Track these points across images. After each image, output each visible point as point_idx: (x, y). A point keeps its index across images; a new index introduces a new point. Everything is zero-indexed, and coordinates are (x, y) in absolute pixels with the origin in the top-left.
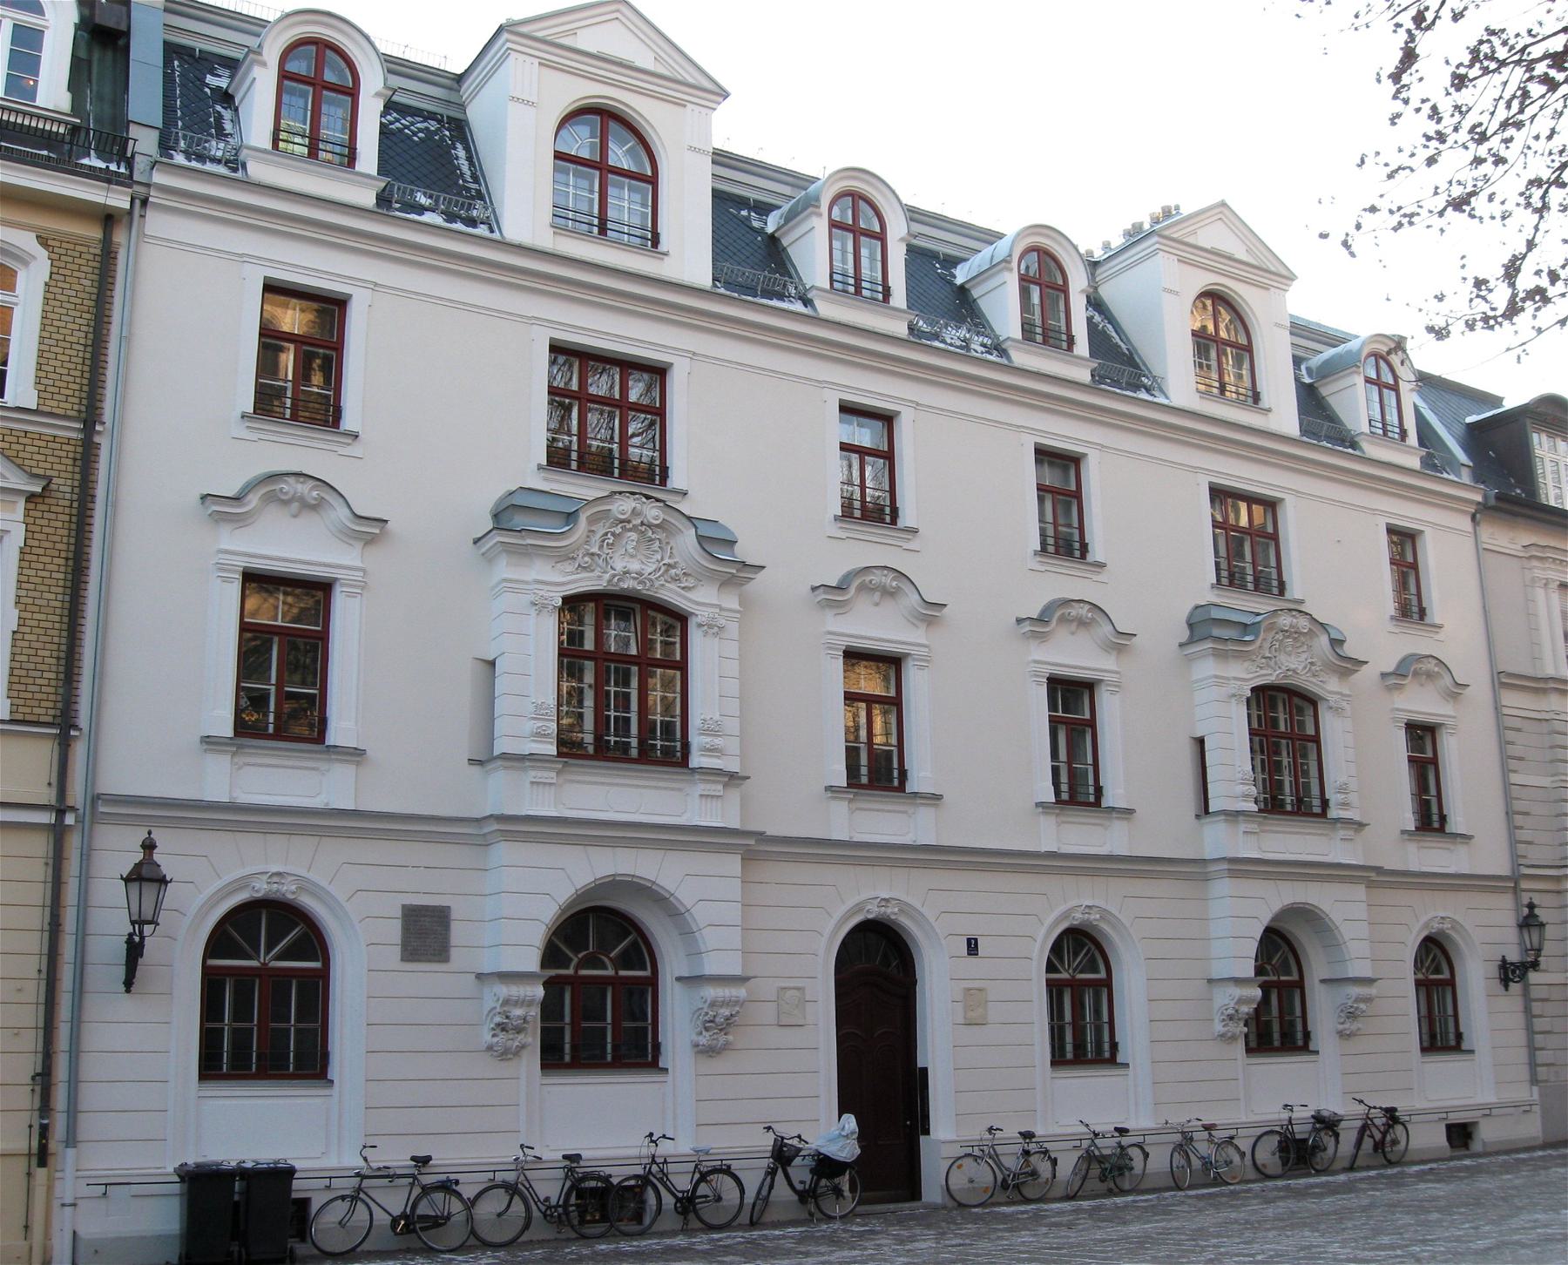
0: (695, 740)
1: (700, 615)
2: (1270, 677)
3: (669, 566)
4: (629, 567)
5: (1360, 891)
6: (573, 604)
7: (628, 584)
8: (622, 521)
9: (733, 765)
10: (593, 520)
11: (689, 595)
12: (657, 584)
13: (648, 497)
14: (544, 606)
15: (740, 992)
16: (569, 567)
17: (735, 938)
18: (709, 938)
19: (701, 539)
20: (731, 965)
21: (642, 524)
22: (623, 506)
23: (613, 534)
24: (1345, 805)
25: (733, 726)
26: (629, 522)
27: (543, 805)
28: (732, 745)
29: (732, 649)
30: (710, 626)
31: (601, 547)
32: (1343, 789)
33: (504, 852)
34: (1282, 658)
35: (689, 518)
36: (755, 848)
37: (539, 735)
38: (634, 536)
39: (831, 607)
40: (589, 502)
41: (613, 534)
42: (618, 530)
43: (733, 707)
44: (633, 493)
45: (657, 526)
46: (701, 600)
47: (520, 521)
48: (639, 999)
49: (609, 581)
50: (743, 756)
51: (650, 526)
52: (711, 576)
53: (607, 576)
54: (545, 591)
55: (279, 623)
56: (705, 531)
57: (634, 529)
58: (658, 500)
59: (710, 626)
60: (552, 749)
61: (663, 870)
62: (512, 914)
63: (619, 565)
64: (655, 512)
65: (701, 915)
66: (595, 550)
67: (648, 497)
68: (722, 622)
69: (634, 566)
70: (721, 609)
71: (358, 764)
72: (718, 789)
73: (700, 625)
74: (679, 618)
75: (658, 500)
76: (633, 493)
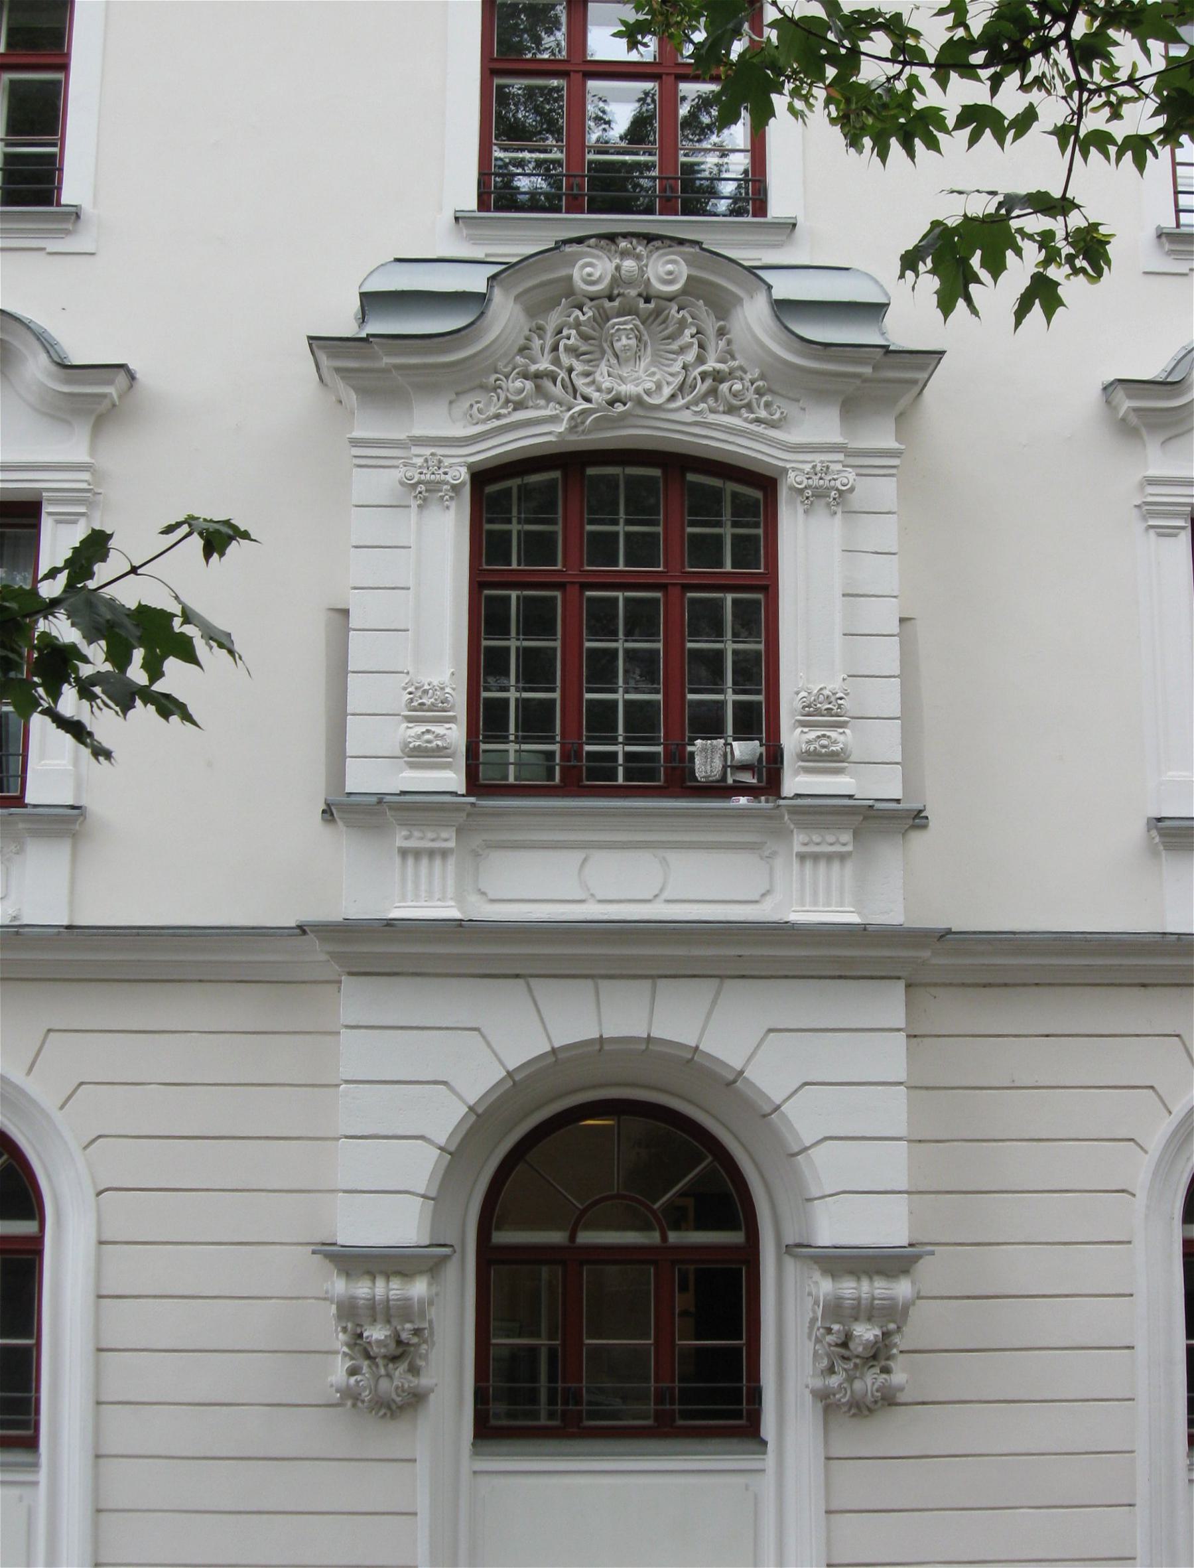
0: (792, 738)
1: (796, 474)
2: (544, 428)
3: (718, 377)
4: (643, 389)
5: (888, 1006)
9: (885, 786)
14: (433, 487)
15: (902, 1289)
17: (893, 1165)
18: (826, 1168)
20: (887, 1227)
22: (594, 269)
24: (826, 759)
25: (886, 697)
27: (426, 895)
28: (885, 741)
32: (825, 713)
33: (356, 1002)
34: (727, 370)
36: (949, 970)
37: (420, 755)
39: (1153, 428)
40: (511, 266)
43: (887, 656)
44: (612, 238)
46: (799, 440)
48: (724, 1299)
49: (572, 429)
50: (910, 763)
56: (786, 287)
60: (453, 779)
61: (680, 1020)
62: (387, 1127)
65: (804, 1119)
66: (544, 365)
71: (75, 837)
72: (844, 840)
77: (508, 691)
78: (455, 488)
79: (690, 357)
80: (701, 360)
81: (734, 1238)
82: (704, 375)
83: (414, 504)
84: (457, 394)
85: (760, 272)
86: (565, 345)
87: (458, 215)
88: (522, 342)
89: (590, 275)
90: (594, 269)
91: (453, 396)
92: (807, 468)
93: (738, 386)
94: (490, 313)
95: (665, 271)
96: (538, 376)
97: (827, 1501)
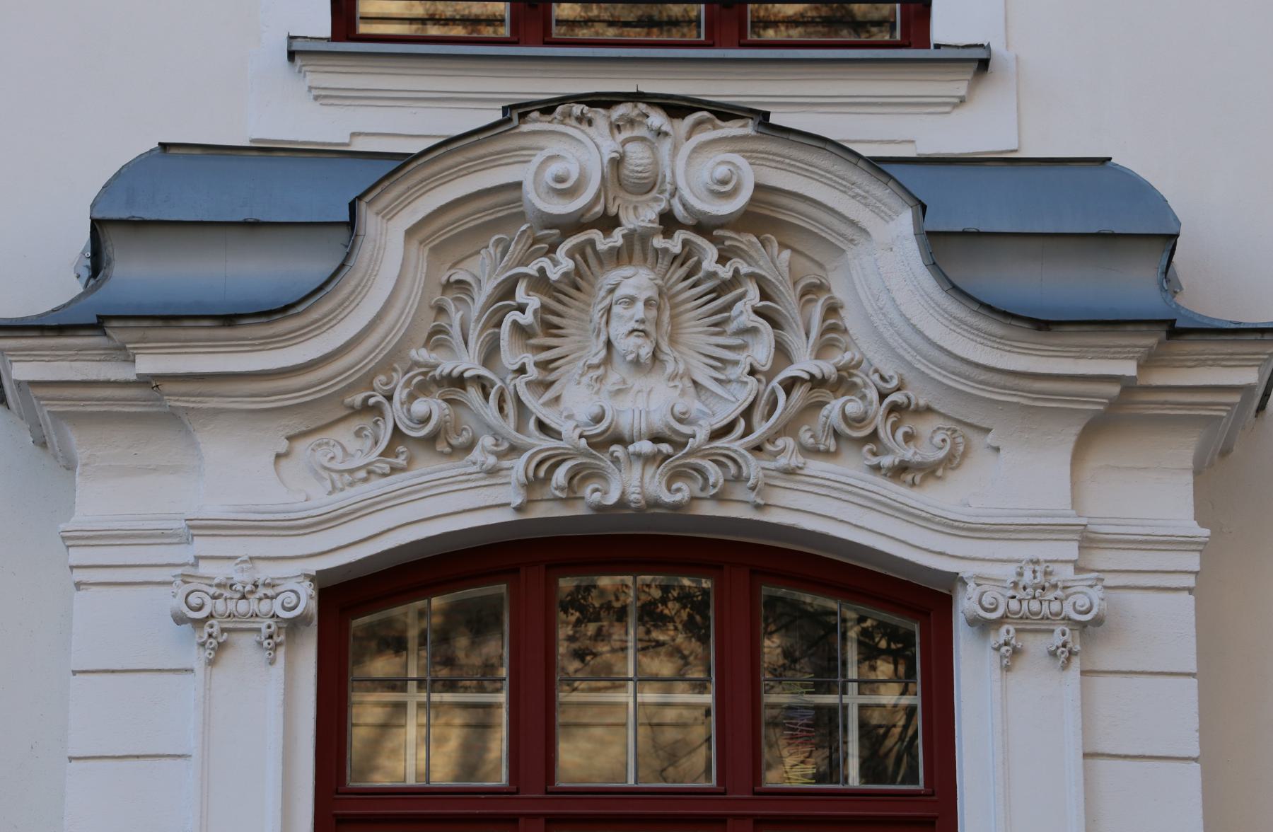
1: (984, 576)
6: (355, 611)
7: (629, 484)
8: (572, 225)
10: (443, 236)
11: (936, 498)
12: (754, 467)
13: (676, 108)
16: (353, 445)
19: (940, 245)
21: (668, 222)
22: (568, 161)
23: (540, 283)
26: (608, 223)
29: (1174, 716)
30: (1030, 623)
31: (491, 354)
35: (877, 165)
38: (636, 280)
41: (540, 283)
42: (560, 266)
44: (605, 101)
45: (750, 220)
46: (984, 510)
47: (956, 100)
49: (534, 484)
51: (704, 227)
52: (1033, 401)
53: (518, 467)
54: (225, 561)
55: (502, 698)
57: (635, 249)
58: (725, 113)
59: (1030, 623)
63: (577, 404)
64: (714, 165)
66: (468, 362)
67: (676, 108)
68: (1086, 598)
69: (647, 403)
70: (1088, 541)
73: (983, 626)
74: (913, 613)
75: (725, 113)
76: (605, 101)
77: (404, 689)
78: (293, 627)
79: (761, 352)
80: (782, 353)
81: (899, 779)
82: (790, 385)
83: (196, 659)
84: (290, 438)
85: (884, 167)
86: (515, 323)
87: (297, 46)
88: (429, 325)
89: (560, 180)
90: (568, 161)
91: (283, 446)
92: (1009, 572)
93: (854, 407)
94: (365, 250)
95: (704, 171)
96: (459, 382)
97: (1087, 726)
